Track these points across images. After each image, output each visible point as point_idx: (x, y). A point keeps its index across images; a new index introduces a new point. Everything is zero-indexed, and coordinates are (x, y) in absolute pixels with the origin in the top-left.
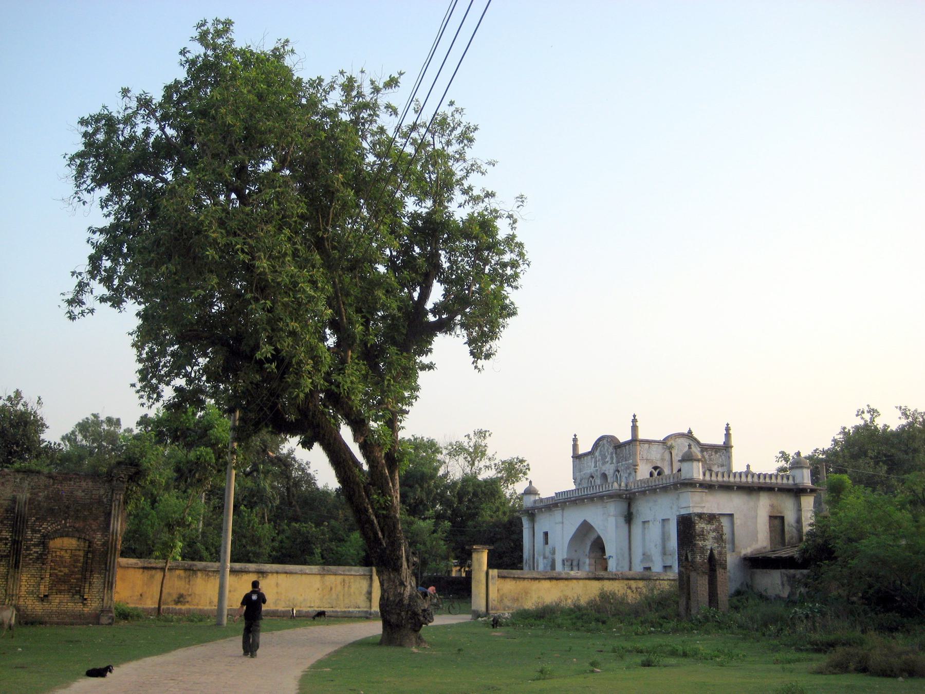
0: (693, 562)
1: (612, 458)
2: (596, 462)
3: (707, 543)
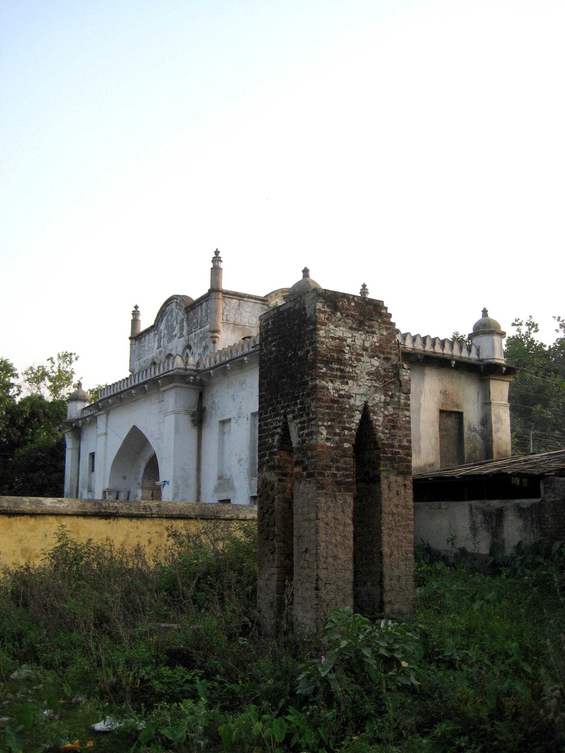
0: (304, 448)
1: (182, 328)
2: (159, 341)
3: (352, 387)
